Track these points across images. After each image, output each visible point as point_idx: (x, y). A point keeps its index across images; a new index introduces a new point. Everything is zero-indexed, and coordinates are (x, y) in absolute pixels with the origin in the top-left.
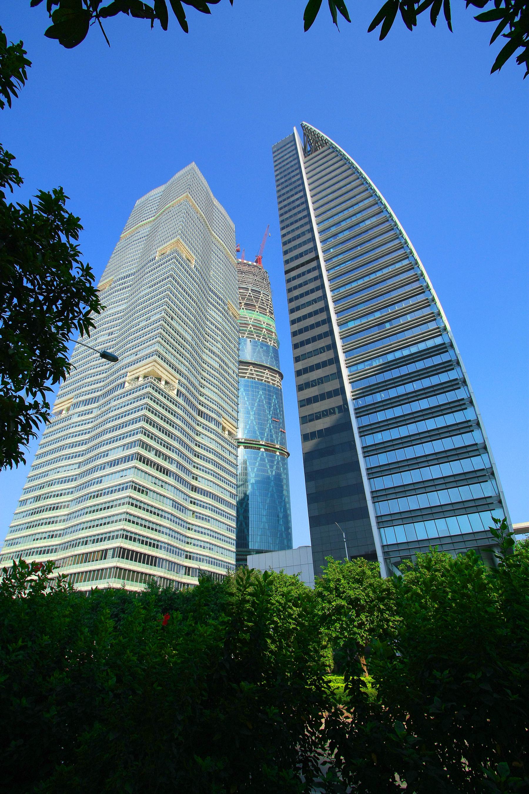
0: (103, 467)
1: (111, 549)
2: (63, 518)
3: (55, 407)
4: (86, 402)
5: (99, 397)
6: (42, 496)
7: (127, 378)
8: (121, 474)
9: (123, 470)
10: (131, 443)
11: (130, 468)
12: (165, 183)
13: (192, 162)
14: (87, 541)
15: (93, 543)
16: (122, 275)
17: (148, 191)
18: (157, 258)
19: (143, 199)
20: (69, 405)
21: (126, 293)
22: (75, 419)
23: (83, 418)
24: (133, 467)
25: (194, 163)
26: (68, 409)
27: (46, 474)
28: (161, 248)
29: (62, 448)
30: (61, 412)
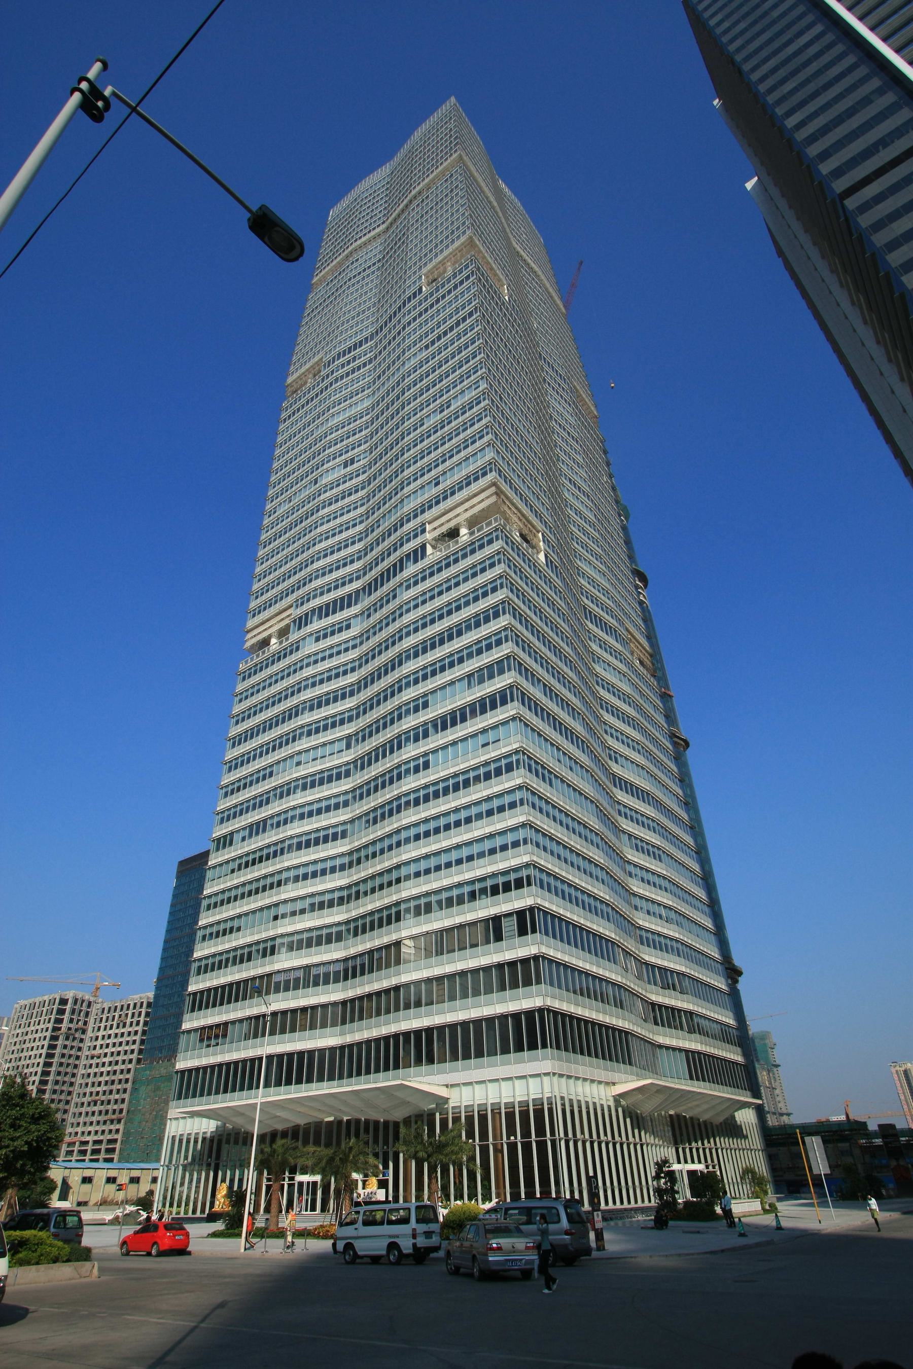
0: (419, 734)
1: (508, 915)
2: (338, 862)
3: (249, 635)
4: (325, 611)
5: (357, 592)
6: (269, 822)
7: (428, 536)
8: (481, 739)
9: (484, 731)
10: (490, 667)
11: (505, 723)
12: (389, 157)
13: (448, 97)
14: (250, 954)
15: (264, 956)
16: (343, 347)
17: (408, 136)
18: (424, 289)
19: (345, 202)
20: (287, 621)
21: (365, 377)
22: (310, 648)
23: (329, 641)
24: (514, 719)
25: (453, 99)
26: (283, 633)
27: (267, 773)
28: (429, 266)
29: (294, 713)
30: (265, 642)
